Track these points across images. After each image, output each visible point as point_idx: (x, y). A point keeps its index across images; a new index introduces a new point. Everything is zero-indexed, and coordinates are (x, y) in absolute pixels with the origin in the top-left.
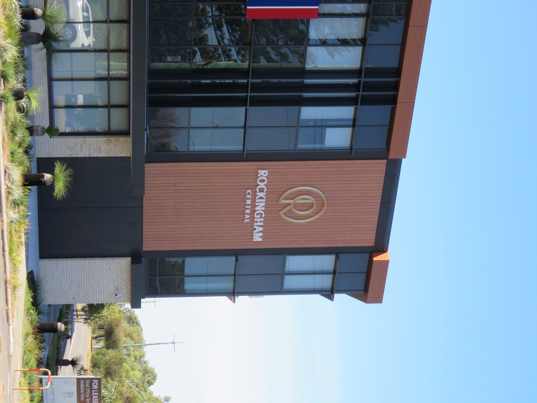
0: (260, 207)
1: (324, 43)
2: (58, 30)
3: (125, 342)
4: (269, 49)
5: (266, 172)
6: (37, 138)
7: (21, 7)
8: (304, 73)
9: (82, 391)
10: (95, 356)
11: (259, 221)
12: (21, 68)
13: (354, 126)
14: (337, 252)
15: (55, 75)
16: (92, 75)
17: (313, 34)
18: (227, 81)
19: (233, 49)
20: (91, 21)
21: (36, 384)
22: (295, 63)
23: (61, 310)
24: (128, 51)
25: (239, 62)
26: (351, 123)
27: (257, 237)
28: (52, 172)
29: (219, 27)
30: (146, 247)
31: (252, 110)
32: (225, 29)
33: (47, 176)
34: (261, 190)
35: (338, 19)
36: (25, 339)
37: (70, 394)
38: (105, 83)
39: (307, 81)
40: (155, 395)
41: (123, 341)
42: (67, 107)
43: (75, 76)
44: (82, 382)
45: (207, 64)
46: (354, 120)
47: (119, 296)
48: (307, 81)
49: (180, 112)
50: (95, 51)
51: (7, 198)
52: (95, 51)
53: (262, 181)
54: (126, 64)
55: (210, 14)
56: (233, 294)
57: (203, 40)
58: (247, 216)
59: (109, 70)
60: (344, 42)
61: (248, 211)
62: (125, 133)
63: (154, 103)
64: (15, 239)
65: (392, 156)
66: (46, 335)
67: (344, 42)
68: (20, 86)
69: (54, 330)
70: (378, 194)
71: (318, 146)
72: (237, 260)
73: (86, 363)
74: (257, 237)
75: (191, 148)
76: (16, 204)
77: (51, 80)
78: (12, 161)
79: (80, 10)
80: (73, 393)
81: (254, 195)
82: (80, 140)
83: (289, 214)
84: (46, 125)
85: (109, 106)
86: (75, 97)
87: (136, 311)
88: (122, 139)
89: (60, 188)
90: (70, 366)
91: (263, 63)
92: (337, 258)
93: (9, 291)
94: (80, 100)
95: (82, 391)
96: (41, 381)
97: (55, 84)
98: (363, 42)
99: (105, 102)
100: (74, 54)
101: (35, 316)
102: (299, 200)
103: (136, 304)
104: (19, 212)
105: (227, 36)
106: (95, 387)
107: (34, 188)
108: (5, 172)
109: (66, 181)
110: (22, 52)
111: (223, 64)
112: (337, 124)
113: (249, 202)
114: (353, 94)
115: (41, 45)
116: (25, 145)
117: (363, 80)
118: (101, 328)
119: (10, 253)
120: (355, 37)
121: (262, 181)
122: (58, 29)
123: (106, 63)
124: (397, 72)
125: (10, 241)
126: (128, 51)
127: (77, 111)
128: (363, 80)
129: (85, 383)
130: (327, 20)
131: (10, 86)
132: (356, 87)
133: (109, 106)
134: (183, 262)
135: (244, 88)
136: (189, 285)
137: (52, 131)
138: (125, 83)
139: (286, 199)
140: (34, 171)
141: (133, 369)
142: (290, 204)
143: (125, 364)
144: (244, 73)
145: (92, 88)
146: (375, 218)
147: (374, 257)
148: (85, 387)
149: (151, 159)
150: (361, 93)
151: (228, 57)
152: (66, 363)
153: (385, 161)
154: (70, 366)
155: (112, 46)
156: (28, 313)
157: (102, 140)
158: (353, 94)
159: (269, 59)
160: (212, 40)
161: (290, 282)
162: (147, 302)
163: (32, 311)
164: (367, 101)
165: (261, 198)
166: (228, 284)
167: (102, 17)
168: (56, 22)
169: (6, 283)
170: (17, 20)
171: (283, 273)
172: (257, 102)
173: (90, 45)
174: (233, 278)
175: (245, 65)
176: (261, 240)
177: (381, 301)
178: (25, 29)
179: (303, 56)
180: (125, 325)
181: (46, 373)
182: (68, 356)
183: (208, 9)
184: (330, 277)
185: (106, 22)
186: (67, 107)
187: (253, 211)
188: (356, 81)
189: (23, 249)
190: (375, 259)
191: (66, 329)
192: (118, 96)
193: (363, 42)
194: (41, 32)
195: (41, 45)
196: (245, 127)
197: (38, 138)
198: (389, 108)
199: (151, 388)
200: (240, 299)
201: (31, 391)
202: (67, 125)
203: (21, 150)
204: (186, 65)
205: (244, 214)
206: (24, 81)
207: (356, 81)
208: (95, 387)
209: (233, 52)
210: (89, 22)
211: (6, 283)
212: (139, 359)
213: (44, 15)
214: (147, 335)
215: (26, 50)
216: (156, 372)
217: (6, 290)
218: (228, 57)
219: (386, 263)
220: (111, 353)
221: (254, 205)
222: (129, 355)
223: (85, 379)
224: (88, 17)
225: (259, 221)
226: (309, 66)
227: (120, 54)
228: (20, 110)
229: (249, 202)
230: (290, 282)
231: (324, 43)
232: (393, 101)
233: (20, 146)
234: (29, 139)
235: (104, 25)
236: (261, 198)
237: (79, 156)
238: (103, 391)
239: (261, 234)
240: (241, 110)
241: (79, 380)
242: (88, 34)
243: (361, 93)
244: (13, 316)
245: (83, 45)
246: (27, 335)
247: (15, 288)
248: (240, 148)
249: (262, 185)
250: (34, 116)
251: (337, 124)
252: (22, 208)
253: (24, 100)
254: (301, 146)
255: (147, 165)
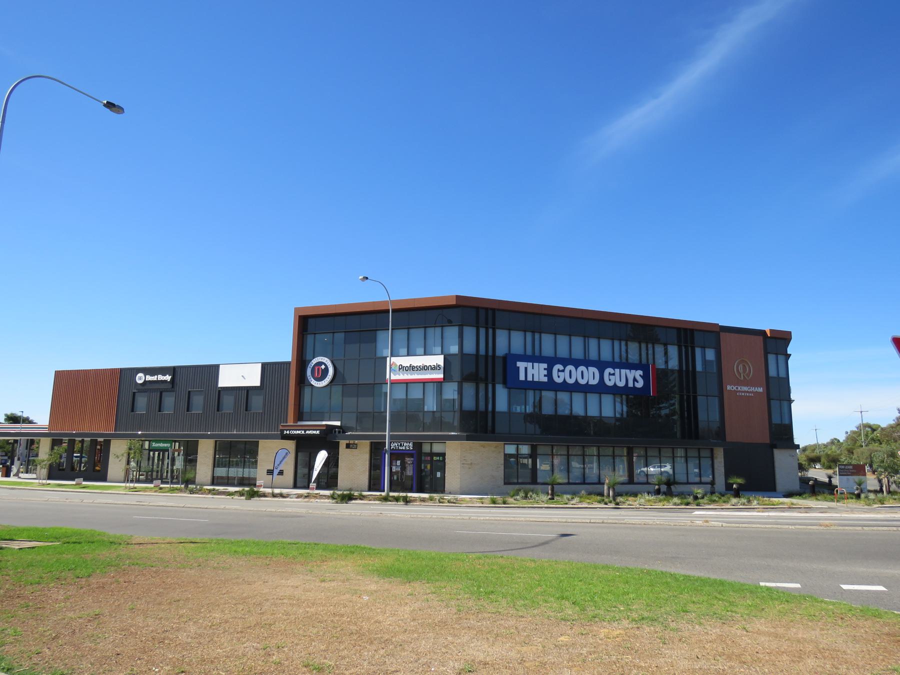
0: (745, 389)
1: (666, 362)
2: (665, 479)
3: (817, 453)
4: (670, 387)
5: (728, 386)
6: (716, 490)
7: (655, 495)
8: (680, 370)
9: (845, 473)
10: (825, 467)
11: (752, 389)
12: (683, 496)
13: (704, 348)
14: (766, 353)
15: (686, 481)
16: (685, 465)
17: (663, 367)
18: (686, 405)
19: (670, 402)
20: (30, 458)
21: (843, 496)
22: (676, 375)
23: (802, 483)
24: (673, 448)
25: (676, 400)
26: (703, 349)
27: (761, 390)
28: (732, 484)
29: (660, 409)
30: (768, 442)
31: (698, 393)
32: (661, 406)
33: (734, 486)
34: (737, 388)
35: (656, 357)
36: (819, 500)
37: (848, 479)
38: (688, 459)
39: (684, 369)
40: (844, 438)
41: (817, 453)
42: (700, 477)
43: (685, 472)
44: (841, 473)
45: (677, 413)
46: (701, 347)
47: (793, 454)
48: (684, 369)
49: (701, 425)
50: (674, 463)
51: (746, 505)
52: (674, 463)
53: (733, 388)
54: (679, 449)
55: (655, 412)
56: (790, 401)
57: (667, 415)
58: (750, 395)
59: (682, 457)
60: (666, 353)
61: (748, 394)
62: (712, 451)
63: (697, 437)
64: (767, 502)
65: (718, 330)
66: (816, 490)
67: (666, 353)
68: (692, 497)
69: (813, 486)
70: (736, 335)
71: (715, 363)
72: (772, 399)
73: (830, 472)
74: (761, 390)
75: (718, 420)
76: (749, 501)
77: (688, 483)
78: (728, 502)
79: (655, 469)
80: (847, 478)
81: (740, 391)
82: (716, 471)
83: (748, 375)
84: (710, 486)
85: (699, 457)
86: (695, 472)
87: (800, 447)
88: (715, 452)
89: (740, 481)
90: (832, 479)
91: (676, 389)
92: (769, 353)
93: (794, 506)
94: (697, 470)
95: (845, 473)
96: (841, 493)
97: (690, 481)
98: (665, 345)
99: (697, 459)
100: (676, 472)
101: (807, 495)
102: (741, 371)
103: (798, 447)
104: (753, 500)
105: (664, 405)
106: (843, 467)
107: (741, 493)
108: (734, 506)
109: (737, 478)
110: (676, 496)
111: (677, 406)
112: (704, 355)
113: (743, 394)
114: (690, 349)
115: (672, 487)
116: (720, 496)
117: (682, 344)
118: (809, 465)
119: (774, 505)
120: (663, 349)
121: (733, 388)
122: (664, 479)
123: (678, 458)
124: (679, 329)
125: (768, 505)
126: (673, 448)
127: (702, 472)
128: (682, 344)
129: (842, 472)
130: (656, 360)
131: (692, 502)
132: (686, 347)
133: (699, 457)
134: (774, 424)
135: (688, 397)
136: (787, 422)
137: (712, 483)
138: (688, 450)
139: (741, 377)
140: (732, 492)
141: (831, 449)
142: (743, 375)
143: (829, 453)
144: (681, 397)
145: (691, 465)
146: (748, 336)
147: (453, 345)
148: (844, 472)
149: (724, 438)
150: (689, 345)
151: (674, 404)
152: (830, 481)
153: (721, 333)
154: (832, 479)
155: (671, 455)
156: (805, 498)
157: (715, 461)
158: (690, 349)
159: (674, 386)
160: (666, 411)
161: (782, 374)
162: (796, 442)
163: (804, 497)
164: (693, 342)
165: (741, 388)
166: (785, 403)
167: (658, 460)
168: (661, 480)
169: (790, 508)
170: (661, 497)
171: (778, 378)
172: (695, 391)
173: (671, 466)
174: (782, 401)
175: (677, 396)
176: (762, 388)
177: (790, 332)
178: (665, 494)
179: (672, 371)
180: (807, 453)
181: (837, 491)
182: (827, 480)
183: (652, 413)
184: (779, 356)
185: (660, 458)
186: (700, 477)
187: (748, 392)
188: (683, 348)
189: (772, 499)
190: (769, 336)
191: (813, 480)
192: (705, 453)
193: (665, 345)
194: (666, 486)
195: (672, 487)
196: (707, 396)
197: (716, 489)
198: (695, 332)
199: (841, 441)
200: (792, 397)
201: (848, 498)
202: (709, 477)
203: (723, 498)
204: (679, 423)
205: (749, 396)
206: (689, 495)
207: (683, 348)
208: (843, 467)
209: (672, 402)
210: (29, 457)
211: (790, 508)
212: (826, 446)
213: (658, 485)
214: (812, 442)
215: (675, 494)
216: (833, 438)
217: (794, 508)
218: (674, 404)
219: (771, 330)
220: (823, 460)
221: (745, 392)
222: (824, 451)
223: (839, 472)
224: (658, 466)
225: (752, 389)
226: (677, 368)
227: (675, 452)
228: (703, 498)
229: (743, 394)
230: (782, 374)
231: (666, 362)
232: (692, 331)
233: (720, 498)
234: (717, 494)
235: (662, 458)
236: (741, 388)
237: (724, 471)
238: (845, 463)
239: (759, 388)
240: (699, 398)
241: (840, 475)
242: (665, 466)
243: (689, 345)
244: (807, 505)
245: (671, 468)
246: (817, 499)
247: (792, 504)
248: (717, 398)
249: (735, 388)
250: (705, 492)
251: (704, 355)
252: (751, 499)
253: (698, 495)
254: (715, 371)
255: (727, 440)
